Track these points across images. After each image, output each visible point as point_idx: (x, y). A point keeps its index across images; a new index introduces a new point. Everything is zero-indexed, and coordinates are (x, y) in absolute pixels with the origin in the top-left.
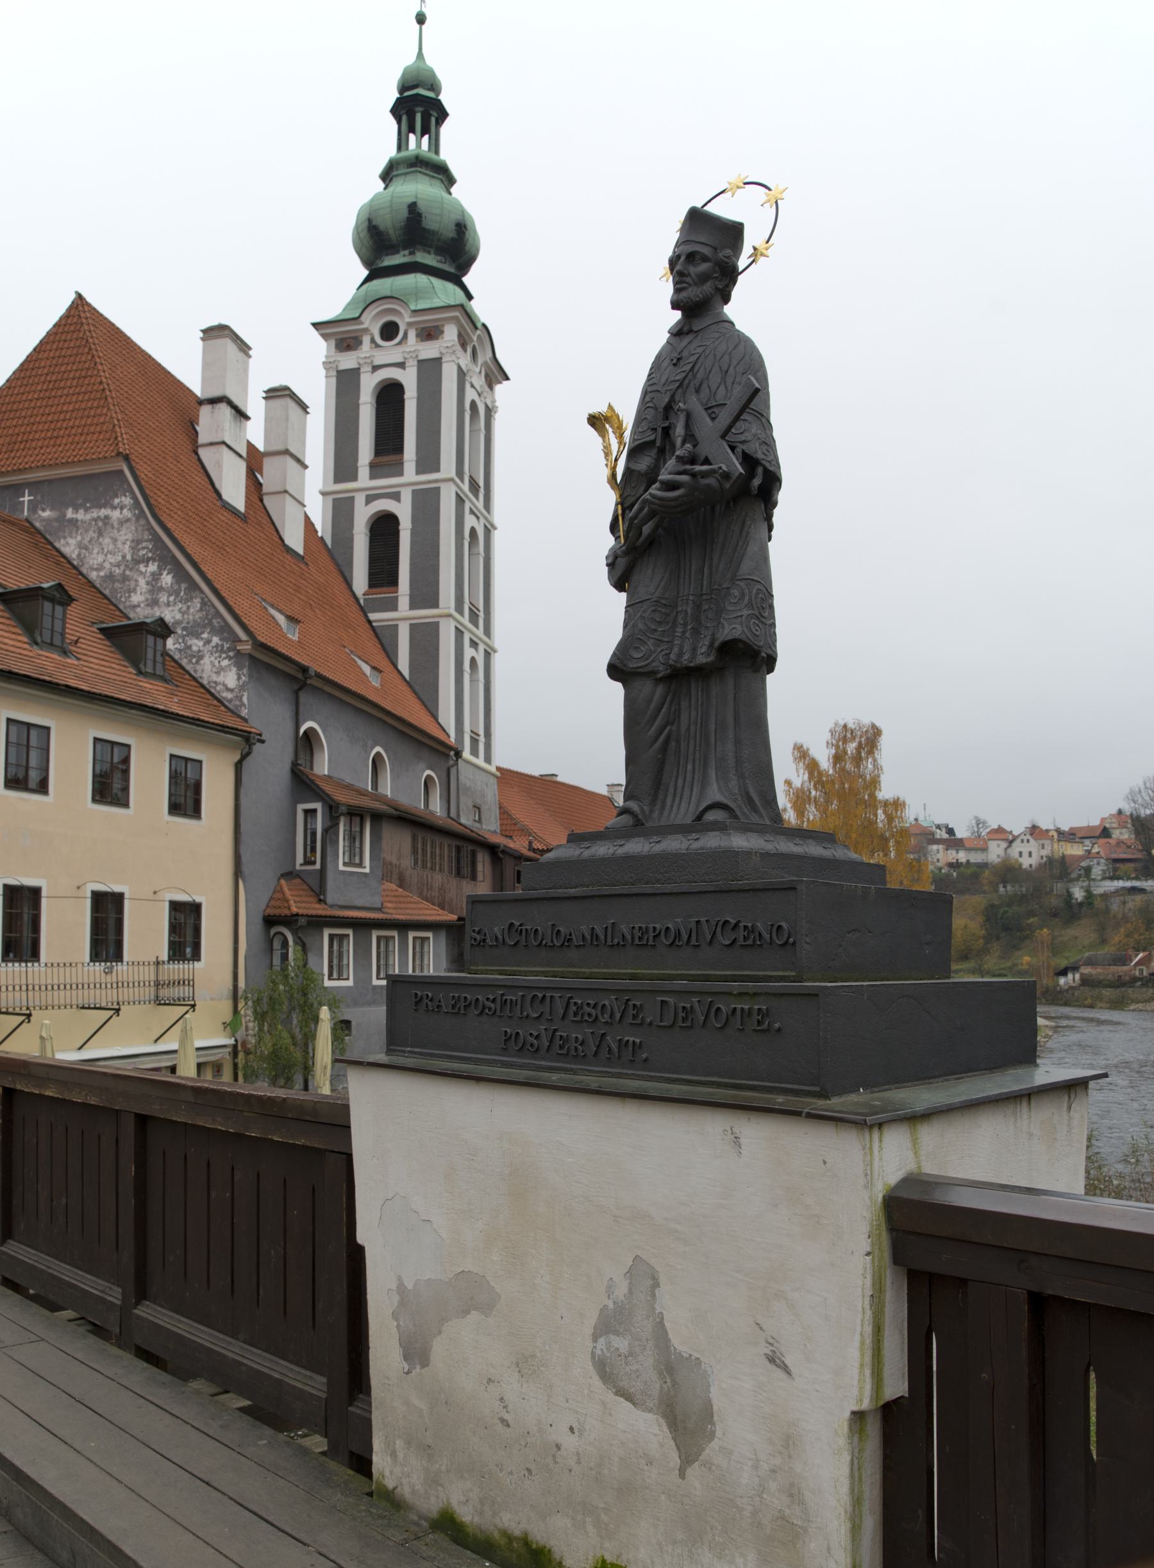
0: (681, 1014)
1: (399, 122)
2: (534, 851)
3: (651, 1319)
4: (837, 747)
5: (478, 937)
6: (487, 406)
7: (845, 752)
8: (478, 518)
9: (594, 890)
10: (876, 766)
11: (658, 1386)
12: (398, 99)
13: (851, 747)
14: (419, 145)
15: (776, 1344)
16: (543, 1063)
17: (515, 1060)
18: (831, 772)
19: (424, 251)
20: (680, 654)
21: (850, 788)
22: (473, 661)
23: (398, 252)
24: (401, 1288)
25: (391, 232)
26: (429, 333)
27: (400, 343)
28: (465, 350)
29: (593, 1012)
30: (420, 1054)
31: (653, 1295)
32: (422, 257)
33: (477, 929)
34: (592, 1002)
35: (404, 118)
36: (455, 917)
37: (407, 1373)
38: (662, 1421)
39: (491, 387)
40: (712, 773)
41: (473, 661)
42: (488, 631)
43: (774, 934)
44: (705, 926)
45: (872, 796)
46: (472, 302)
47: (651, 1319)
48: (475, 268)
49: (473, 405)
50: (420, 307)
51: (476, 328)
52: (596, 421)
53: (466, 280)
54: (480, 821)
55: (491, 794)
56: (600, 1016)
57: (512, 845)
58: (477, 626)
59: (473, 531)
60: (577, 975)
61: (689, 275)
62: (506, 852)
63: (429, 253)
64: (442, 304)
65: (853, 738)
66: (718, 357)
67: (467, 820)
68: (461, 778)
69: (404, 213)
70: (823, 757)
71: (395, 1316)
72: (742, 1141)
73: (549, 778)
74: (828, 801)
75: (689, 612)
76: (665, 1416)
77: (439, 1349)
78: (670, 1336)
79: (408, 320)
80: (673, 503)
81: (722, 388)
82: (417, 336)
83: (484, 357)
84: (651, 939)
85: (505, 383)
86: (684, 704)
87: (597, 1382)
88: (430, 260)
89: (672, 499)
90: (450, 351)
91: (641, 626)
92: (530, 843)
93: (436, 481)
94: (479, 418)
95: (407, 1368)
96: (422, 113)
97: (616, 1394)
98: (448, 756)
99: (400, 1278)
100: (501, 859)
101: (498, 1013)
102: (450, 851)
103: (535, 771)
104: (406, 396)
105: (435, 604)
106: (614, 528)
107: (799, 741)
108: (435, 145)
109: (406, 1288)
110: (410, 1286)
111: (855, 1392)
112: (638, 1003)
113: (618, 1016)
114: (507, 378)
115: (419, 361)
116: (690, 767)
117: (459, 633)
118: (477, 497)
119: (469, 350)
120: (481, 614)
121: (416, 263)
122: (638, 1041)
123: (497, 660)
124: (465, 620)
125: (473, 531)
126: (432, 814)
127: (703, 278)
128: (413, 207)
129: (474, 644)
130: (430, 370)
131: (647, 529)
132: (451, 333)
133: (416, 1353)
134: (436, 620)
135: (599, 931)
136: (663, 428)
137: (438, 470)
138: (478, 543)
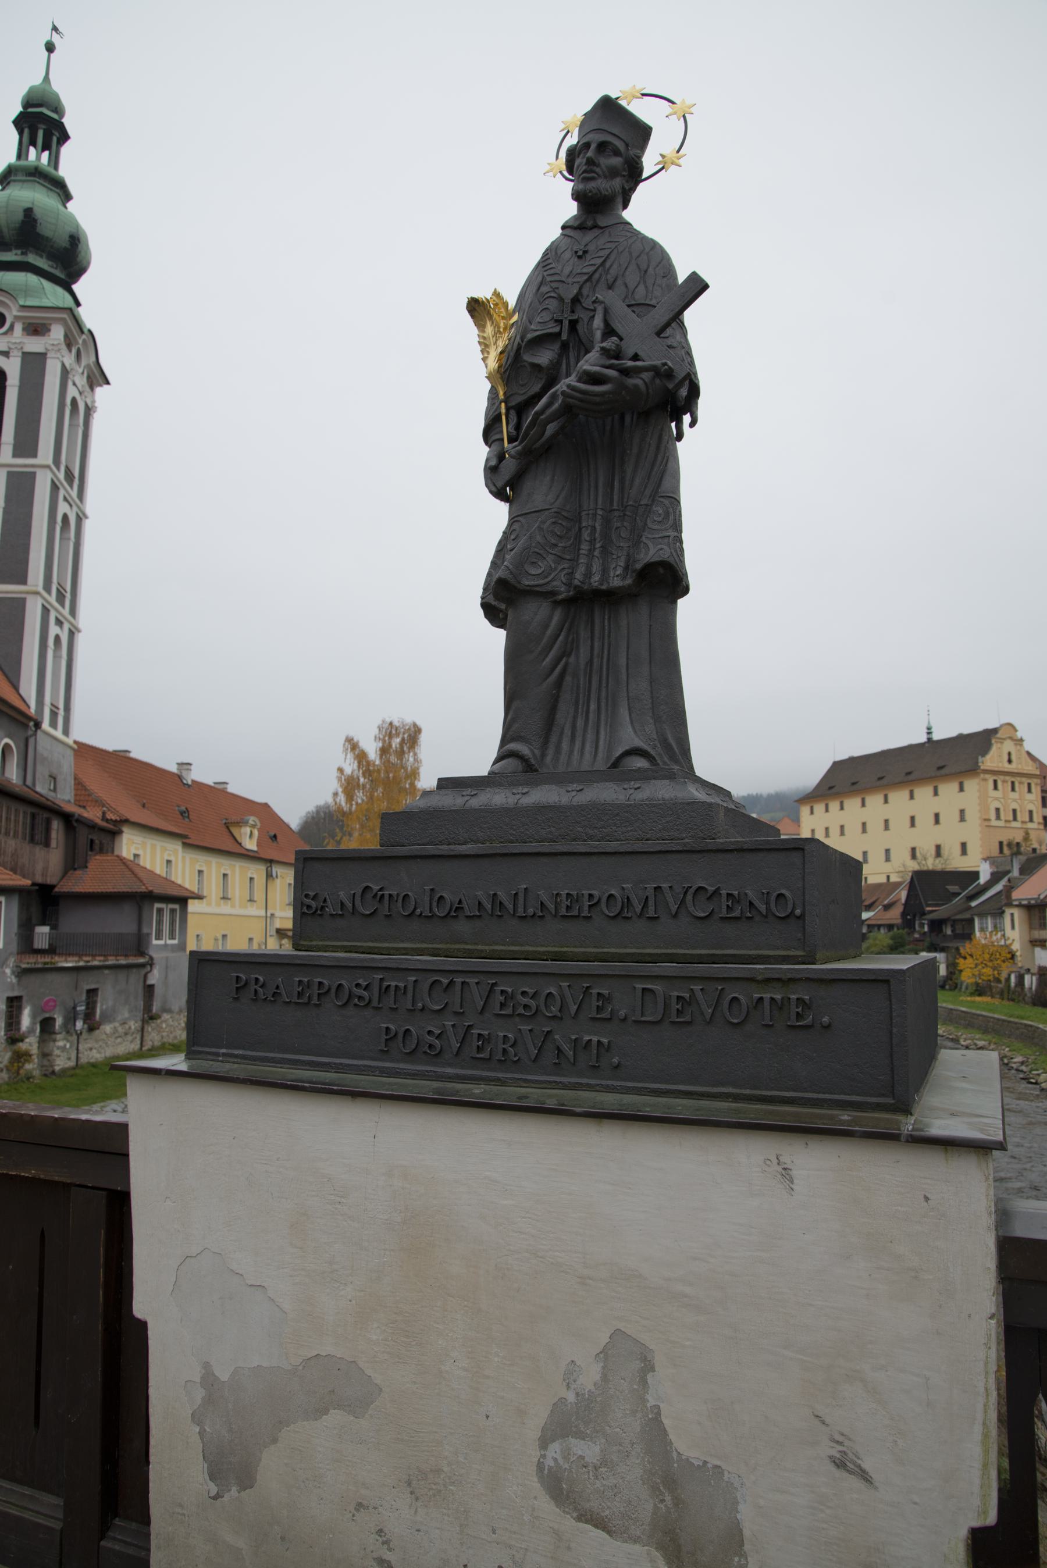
0: (675, 1006)
1: (21, 133)
2: (107, 821)
3: (639, 1415)
4: (384, 741)
5: (314, 904)
6: (86, 405)
7: (390, 745)
8: (71, 506)
9: (498, 847)
10: (416, 760)
11: (649, 1506)
12: (21, 113)
13: (396, 742)
14: (38, 158)
15: (847, 1443)
16: (449, 1070)
17: (402, 1066)
18: (378, 762)
19: (37, 254)
20: (588, 574)
21: (394, 777)
22: (57, 638)
23: (10, 250)
24: (209, 1379)
25: (5, 230)
26: (36, 329)
27: (5, 333)
28: (70, 351)
29: (533, 1003)
30: (243, 1057)
31: (644, 1382)
32: (32, 258)
33: (312, 894)
34: (531, 991)
35: (26, 131)
36: (29, 882)
37: (215, 1498)
38: (657, 1554)
39: (92, 388)
40: (624, 712)
41: (57, 638)
42: (73, 612)
43: (435, 904)
44: (668, 895)
45: (412, 785)
46: (80, 309)
47: (639, 1415)
48: (84, 279)
49: (74, 401)
50: (28, 303)
51: (82, 332)
52: (476, 308)
53: (76, 287)
54: (55, 790)
55: (67, 766)
56: (543, 1008)
57: (86, 815)
58: (63, 606)
59: (65, 517)
60: (470, 954)
61: (598, 165)
62: (81, 821)
63: (41, 257)
64: (50, 305)
65: (397, 735)
66: (635, 255)
67: (42, 788)
68: (39, 748)
69: (20, 216)
70: (372, 749)
71: (196, 1418)
72: (794, 1173)
73: (122, 754)
74: (373, 789)
75: (598, 528)
76: (661, 1547)
77: (271, 1465)
78: (672, 1437)
79: (15, 313)
80: (597, 399)
81: (641, 287)
82: (24, 329)
83: (88, 359)
84: (586, 908)
85: (106, 387)
86: (584, 634)
87: (545, 1504)
88: (42, 263)
89: (596, 394)
90: (56, 348)
91: (539, 538)
92: (104, 813)
93: (33, 466)
94: (79, 416)
95: (214, 1490)
96: (45, 130)
97: (579, 1519)
98: (26, 726)
99: (207, 1366)
100: (74, 828)
101: (375, 1003)
102: (25, 817)
103: (110, 747)
104: (8, 383)
105: (23, 581)
106: (489, 433)
107: (351, 734)
108: (55, 161)
109: (217, 1378)
110: (224, 1376)
111: (976, 1501)
112: (605, 992)
113: (574, 1008)
114: (108, 383)
115: (24, 353)
116: (593, 706)
117: (46, 611)
118: (71, 486)
119: (74, 350)
120: (68, 596)
121: (28, 263)
122: (605, 1041)
123: (81, 640)
124: (53, 599)
125: (65, 517)
126: (9, 781)
127: (613, 173)
128: (28, 212)
129: (59, 623)
130: (33, 364)
131: (551, 429)
132: (57, 333)
133: (231, 1468)
134: (23, 596)
135: (502, 896)
136: (570, 321)
137: (35, 456)
138: (70, 529)
